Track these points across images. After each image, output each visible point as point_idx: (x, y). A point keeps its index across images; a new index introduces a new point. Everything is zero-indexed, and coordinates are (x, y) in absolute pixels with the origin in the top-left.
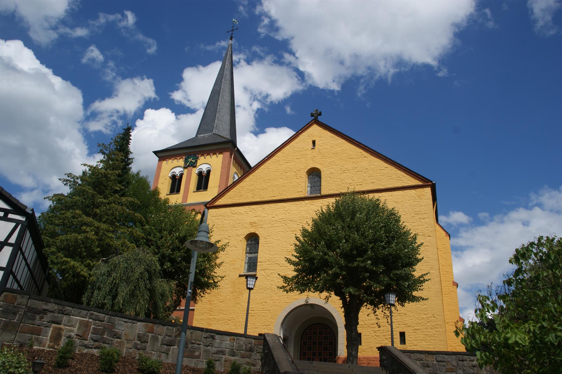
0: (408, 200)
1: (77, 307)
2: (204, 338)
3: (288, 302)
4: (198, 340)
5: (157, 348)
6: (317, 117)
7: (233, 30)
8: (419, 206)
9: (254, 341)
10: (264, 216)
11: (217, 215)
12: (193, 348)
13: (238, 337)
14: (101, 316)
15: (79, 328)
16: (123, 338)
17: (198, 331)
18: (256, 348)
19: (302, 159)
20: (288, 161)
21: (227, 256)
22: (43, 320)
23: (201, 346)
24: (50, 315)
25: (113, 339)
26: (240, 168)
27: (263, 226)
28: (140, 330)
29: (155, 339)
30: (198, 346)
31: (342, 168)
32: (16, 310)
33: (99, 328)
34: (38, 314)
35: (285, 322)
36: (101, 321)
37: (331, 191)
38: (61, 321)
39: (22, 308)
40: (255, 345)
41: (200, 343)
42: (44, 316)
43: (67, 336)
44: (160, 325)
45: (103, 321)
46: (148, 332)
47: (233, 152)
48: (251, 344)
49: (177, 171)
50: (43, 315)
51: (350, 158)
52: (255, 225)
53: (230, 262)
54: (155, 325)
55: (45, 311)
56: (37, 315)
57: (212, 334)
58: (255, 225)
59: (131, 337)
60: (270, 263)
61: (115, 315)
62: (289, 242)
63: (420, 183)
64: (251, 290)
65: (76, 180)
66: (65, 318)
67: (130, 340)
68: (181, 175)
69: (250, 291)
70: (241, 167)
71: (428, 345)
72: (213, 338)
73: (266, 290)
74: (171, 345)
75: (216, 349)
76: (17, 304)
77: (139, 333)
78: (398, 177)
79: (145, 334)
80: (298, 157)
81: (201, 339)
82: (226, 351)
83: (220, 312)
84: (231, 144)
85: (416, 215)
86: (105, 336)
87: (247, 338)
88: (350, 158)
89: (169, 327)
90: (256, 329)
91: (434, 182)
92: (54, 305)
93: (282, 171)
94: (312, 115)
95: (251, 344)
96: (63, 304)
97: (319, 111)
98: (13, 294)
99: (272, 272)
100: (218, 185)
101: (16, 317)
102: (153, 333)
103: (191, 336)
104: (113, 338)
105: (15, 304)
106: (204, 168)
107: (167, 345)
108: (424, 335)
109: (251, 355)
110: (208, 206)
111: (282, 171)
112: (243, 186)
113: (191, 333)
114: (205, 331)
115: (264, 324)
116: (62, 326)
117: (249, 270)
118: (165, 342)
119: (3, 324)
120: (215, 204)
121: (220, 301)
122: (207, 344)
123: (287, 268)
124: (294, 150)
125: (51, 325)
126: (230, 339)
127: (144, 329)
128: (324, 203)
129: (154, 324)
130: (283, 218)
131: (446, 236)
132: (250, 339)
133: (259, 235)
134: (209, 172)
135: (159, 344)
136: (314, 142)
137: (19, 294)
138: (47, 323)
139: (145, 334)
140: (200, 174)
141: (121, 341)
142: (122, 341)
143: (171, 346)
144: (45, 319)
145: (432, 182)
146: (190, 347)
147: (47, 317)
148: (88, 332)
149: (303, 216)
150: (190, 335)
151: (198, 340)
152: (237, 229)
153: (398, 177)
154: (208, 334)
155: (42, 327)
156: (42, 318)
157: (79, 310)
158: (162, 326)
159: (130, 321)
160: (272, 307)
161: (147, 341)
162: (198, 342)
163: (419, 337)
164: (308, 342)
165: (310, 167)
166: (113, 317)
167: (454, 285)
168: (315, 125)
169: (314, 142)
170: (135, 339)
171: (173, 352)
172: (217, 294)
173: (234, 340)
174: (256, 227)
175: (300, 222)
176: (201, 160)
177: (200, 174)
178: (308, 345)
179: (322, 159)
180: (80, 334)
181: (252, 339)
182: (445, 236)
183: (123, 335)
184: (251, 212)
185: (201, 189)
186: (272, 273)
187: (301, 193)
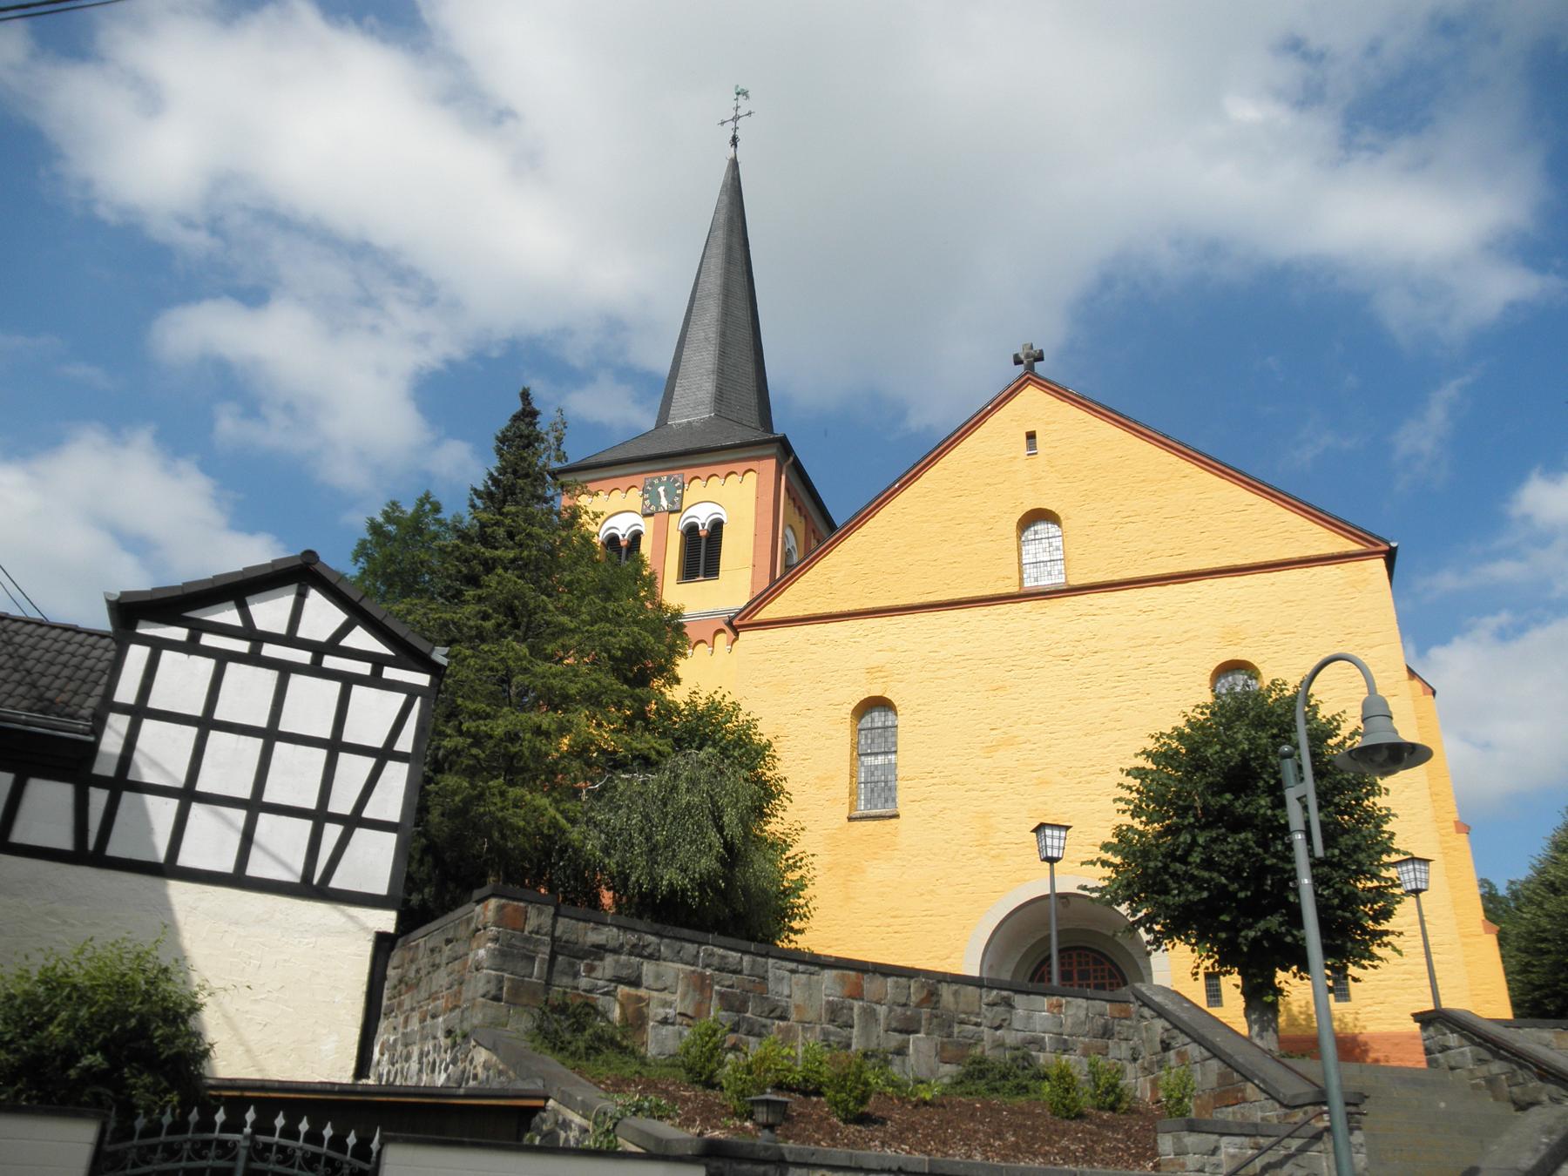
0: (1323, 596)
1: (671, 934)
2: (988, 1005)
3: (999, 889)
4: (971, 1013)
5: (876, 1042)
6: (1030, 368)
7: (736, 118)
8: (1356, 612)
9: (1108, 1006)
10: (906, 648)
11: (767, 649)
12: (965, 1037)
13: (1069, 999)
14: (732, 956)
15: (684, 996)
16: (793, 1016)
17: (970, 988)
18: (1117, 1028)
20: (961, 493)
21: (806, 763)
22: (593, 975)
23: (982, 1028)
24: (609, 959)
25: (768, 1022)
26: (797, 512)
27: (906, 677)
28: (828, 992)
29: (870, 1015)
30: (974, 1027)
31: (1120, 508)
32: (532, 947)
33: (732, 993)
34: (582, 959)
35: (990, 948)
36: (734, 972)
37: (1094, 575)
38: (639, 977)
39: (543, 943)
40: (1114, 1018)
41: (979, 1020)
42: (596, 963)
43: (659, 1018)
44: (878, 975)
45: (740, 972)
46: (849, 997)
47: (784, 470)
48: (1102, 1015)
50: (595, 959)
51: (1143, 481)
52: (882, 674)
53: (817, 781)
54: (865, 977)
55: (599, 951)
56: (578, 962)
57: (1005, 993)
58: (882, 674)
59: (811, 1015)
60: (934, 781)
61: (764, 952)
63: (1354, 547)
64: (1421, 895)
66: (648, 968)
67: (809, 1023)
69: (1417, 897)
70: (799, 509)
71: (1419, 1001)
72: (1009, 1004)
73: (931, 856)
74: (911, 1029)
75: (1020, 1035)
76: (531, 933)
77: (828, 1002)
78: (1286, 531)
79: (843, 1002)
80: (988, 481)
81: (980, 1008)
82: (1043, 1038)
85: (1349, 636)
86: (748, 1015)
87: (1092, 999)
88: (1143, 481)
89: (900, 979)
91: (1394, 544)
92: (615, 930)
93: (947, 520)
94: (1018, 361)
95: (1102, 1015)
96: (638, 927)
97: (1036, 348)
98: (516, 903)
99: (944, 805)
100: (751, 562)
101: (534, 967)
102: (863, 999)
103: (957, 1003)
104: (767, 1017)
105: (526, 933)
106: (702, 515)
107: (900, 1032)
108: (1404, 973)
109: (1107, 1047)
111: (947, 520)
112: (835, 566)
113: (956, 993)
114: (987, 987)
115: (931, 955)
116: (642, 992)
118: (894, 1024)
119: (508, 989)
120: (756, 618)
122: (997, 1022)
124: (974, 460)
125: (616, 987)
126: (1051, 1005)
127: (839, 989)
128: (1076, 608)
129: (860, 975)
130: (962, 652)
131: (1425, 694)
132: (1098, 1002)
133: (896, 704)
134: (717, 526)
135: (881, 1028)
136: (1031, 436)
137: (531, 902)
138: (607, 983)
139: (843, 1002)
140: (691, 531)
141: (787, 1027)
142: (792, 1026)
143: (909, 1032)
144: (598, 973)
145: (1387, 543)
146: (955, 1035)
147: (608, 965)
148: (707, 1006)
149: (1020, 646)
150: (951, 999)
151: (971, 1013)
152: (828, 687)
153: (1286, 531)
154: (995, 992)
155: (595, 996)
156: (591, 969)
157: (677, 945)
158: (881, 979)
159: (801, 968)
160: (951, 906)
161: (850, 1022)
162: (974, 1019)
163: (1390, 979)
165: (1029, 509)
166: (759, 959)
167: (1458, 831)
169: (1031, 436)
170: (820, 1020)
171: (916, 1050)
173: (1061, 1006)
174: (885, 680)
176: (694, 491)
177: (691, 531)
179: (1060, 486)
180: (690, 1013)
181: (1104, 1003)
182: (1421, 693)
183: (792, 1009)
185: (698, 576)
186: (945, 808)
187: (1007, 581)
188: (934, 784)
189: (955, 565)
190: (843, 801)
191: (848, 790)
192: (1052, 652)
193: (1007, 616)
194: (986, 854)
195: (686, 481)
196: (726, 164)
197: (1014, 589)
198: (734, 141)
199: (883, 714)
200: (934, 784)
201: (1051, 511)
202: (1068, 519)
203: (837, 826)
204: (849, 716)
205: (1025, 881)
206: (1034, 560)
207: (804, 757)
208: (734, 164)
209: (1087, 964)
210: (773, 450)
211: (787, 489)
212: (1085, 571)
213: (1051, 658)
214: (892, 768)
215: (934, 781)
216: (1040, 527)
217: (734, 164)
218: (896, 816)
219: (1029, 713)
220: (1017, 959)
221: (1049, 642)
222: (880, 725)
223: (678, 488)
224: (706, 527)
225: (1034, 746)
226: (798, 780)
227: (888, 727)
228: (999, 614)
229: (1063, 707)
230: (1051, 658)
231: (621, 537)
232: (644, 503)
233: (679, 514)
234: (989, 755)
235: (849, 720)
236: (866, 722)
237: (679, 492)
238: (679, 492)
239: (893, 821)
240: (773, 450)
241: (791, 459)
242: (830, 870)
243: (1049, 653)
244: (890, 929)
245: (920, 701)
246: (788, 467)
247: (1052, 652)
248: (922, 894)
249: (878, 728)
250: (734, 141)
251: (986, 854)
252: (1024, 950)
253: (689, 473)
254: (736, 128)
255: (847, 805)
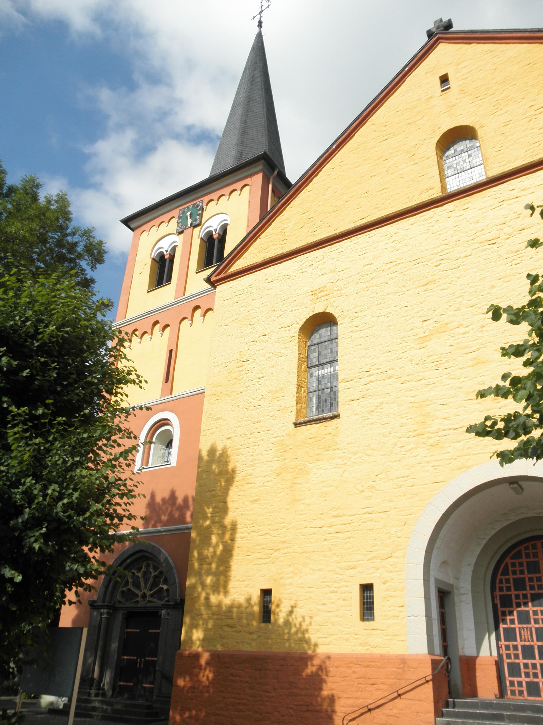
11: (235, 294)
19: (419, 122)
21: (261, 381)
49: (165, 246)
60: (371, 378)
62: (419, 314)
65: (214, 599)
68: (174, 249)
83: (253, 529)
84: (263, 161)
90: (352, 572)
97: (445, 19)
110: (213, 279)
112: (288, 219)
117: (320, 407)
121: (252, 499)
123: (422, 382)
128: (498, 196)
133: (336, 316)
149: (445, 242)
164: (522, 572)
168: (441, 44)
172: (243, 480)
175: (441, 258)
178: (521, 564)
184: (312, 267)
188: (371, 382)
189: (384, 191)
190: (290, 409)
191: (295, 399)
192: (477, 240)
193: (432, 220)
194: (424, 443)
195: (205, 204)
196: (254, 37)
197: (436, 193)
198: (260, 24)
199: (329, 329)
200: (371, 382)
201: (466, 127)
202: (482, 127)
203: (285, 433)
204: (297, 334)
205: (468, 467)
206: (456, 172)
207: (260, 375)
208: (260, 36)
209: (522, 572)
210: (260, 166)
211: (273, 191)
212: (504, 163)
213: (477, 246)
214: (334, 376)
215: (371, 378)
216: (461, 146)
217: (260, 36)
218: (337, 417)
219: (460, 299)
220: (478, 552)
221: (474, 232)
222: (326, 338)
223: (199, 210)
224: (217, 232)
225: (467, 329)
226: (255, 396)
227: (333, 339)
228: (425, 220)
229: (493, 287)
230: (477, 246)
231: (165, 253)
232: (178, 226)
233: (199, 228)
234: (423, 345)
235: (296, 338)
236: (316, 338)
237: (200, 212)
238: (200, 212)
239: (334, 421)
240: (260, 166)
241: (276, 172)
242: (279, 474)
243: (475, 241)
244: (332, 530)
245: (357, 309)
246: (274, 178)
247: (477, 240)
248: (362, 491)
249: (325, 342)
250: (260, 24)
251: (424, 443)
252: (484, 542)
253: (206, 199)
254: (261, 17)
255: (294, 413)
